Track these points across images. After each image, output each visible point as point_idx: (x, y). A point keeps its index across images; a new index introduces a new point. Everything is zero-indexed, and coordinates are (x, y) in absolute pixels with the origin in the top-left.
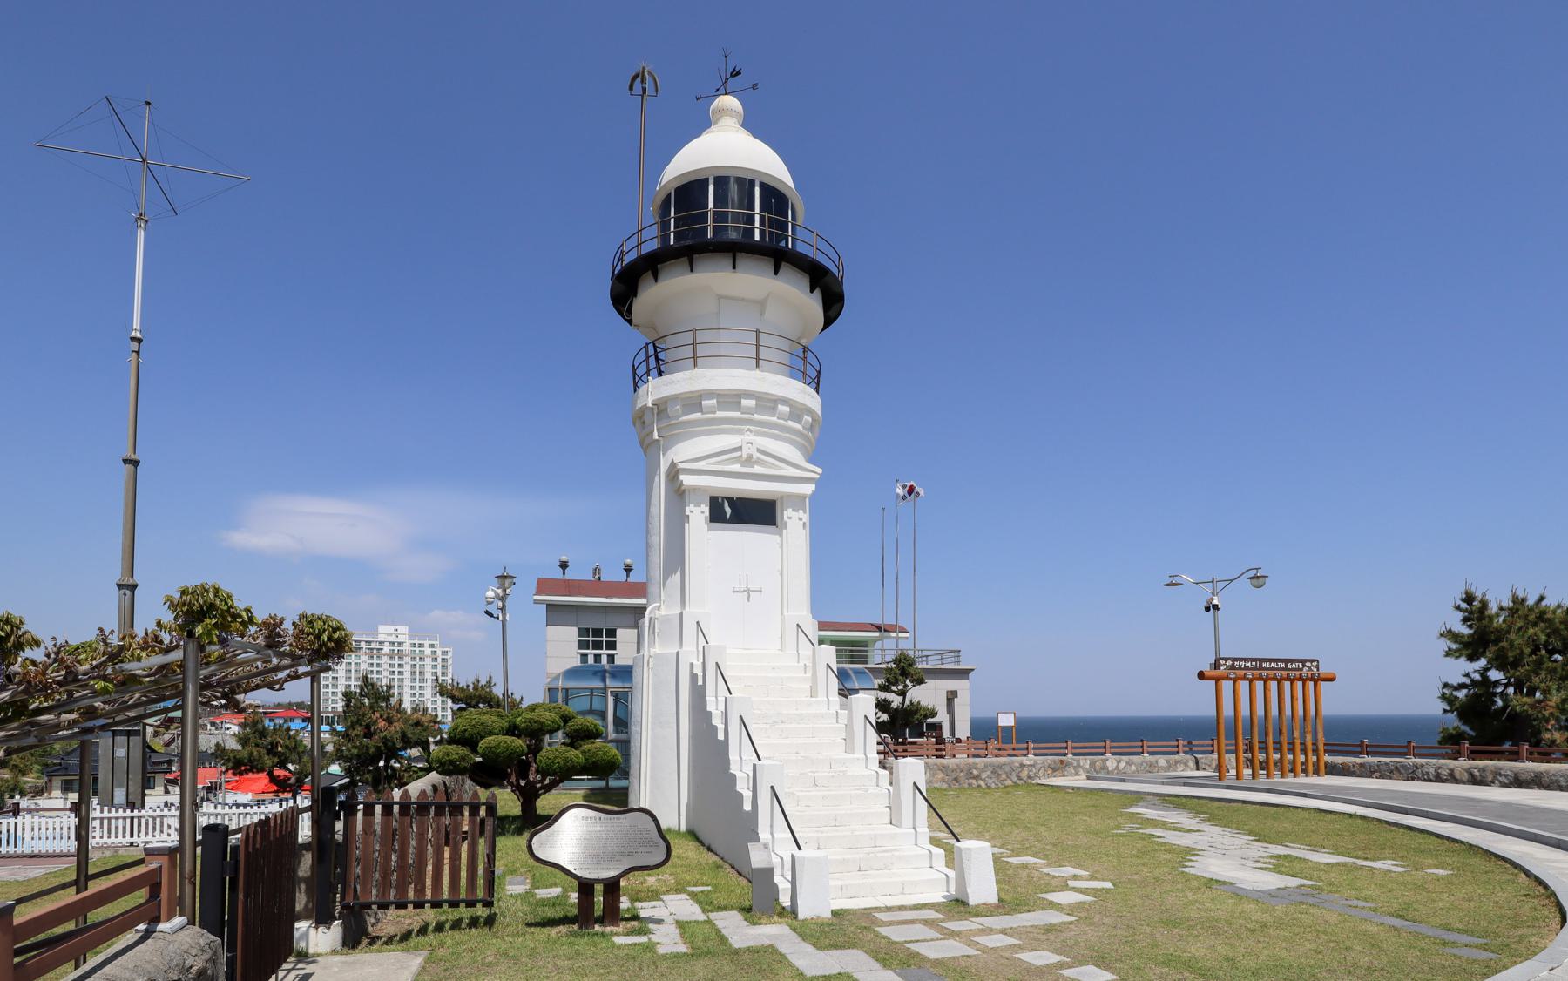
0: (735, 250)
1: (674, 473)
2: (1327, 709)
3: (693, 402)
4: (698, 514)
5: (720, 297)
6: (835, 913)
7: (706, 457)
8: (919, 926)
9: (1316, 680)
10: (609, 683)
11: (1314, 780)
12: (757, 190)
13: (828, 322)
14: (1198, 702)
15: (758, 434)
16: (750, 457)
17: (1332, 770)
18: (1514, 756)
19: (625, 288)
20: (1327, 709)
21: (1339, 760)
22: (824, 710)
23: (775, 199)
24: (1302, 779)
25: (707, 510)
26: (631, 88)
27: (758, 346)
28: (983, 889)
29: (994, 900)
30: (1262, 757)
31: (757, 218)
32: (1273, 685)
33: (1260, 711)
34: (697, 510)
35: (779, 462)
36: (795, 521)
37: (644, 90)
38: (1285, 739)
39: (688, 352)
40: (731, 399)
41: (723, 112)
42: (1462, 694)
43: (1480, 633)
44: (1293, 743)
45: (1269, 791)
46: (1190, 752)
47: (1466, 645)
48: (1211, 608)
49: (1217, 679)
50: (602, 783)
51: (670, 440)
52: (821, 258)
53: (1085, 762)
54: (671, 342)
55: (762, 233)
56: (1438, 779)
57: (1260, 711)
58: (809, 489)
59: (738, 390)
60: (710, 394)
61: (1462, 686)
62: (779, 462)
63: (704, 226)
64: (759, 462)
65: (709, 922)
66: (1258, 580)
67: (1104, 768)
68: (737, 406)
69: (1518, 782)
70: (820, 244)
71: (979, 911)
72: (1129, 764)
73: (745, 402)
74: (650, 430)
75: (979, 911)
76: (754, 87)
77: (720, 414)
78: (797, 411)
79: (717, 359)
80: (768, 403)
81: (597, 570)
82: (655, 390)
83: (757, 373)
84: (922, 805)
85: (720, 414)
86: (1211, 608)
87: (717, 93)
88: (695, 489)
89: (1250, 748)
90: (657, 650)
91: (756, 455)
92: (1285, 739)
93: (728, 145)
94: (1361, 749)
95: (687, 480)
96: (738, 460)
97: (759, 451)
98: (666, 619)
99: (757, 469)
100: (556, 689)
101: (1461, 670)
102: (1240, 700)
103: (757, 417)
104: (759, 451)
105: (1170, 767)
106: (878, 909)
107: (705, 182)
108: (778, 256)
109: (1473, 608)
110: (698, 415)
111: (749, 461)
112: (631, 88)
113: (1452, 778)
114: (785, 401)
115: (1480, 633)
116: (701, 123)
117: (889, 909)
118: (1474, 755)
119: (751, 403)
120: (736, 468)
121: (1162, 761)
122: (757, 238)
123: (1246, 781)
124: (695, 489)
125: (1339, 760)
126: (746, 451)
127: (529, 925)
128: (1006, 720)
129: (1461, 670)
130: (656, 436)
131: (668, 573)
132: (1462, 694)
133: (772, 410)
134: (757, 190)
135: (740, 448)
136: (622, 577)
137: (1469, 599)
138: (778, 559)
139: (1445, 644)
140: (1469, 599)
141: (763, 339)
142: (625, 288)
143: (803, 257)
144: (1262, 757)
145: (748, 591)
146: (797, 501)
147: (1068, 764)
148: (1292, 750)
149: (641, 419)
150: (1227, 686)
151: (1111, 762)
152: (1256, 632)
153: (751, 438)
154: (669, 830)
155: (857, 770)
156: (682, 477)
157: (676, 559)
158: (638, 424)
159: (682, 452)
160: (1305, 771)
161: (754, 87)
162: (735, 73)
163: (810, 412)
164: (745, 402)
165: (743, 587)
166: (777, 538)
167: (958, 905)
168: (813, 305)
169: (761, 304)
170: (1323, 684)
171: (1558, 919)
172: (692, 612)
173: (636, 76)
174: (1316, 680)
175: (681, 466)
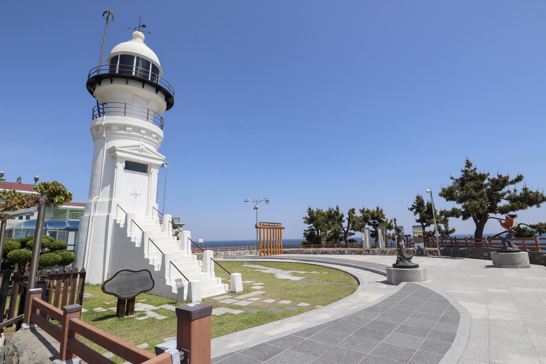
0: (143, 81)
1: (112, 152)
2: (284, 238)
3: (123, 127)
4: (121, 166)
5: (134, 95)
6: (203, 300)
7: (126, 146)
8: (229, 299)
9: (281, 229)
10: (48, 227)
11: (280, 255)
12: (135, 60)
13: (167, 110)
14: (252, 235)
15: (145, 142)
16: (142, 149)
17: (285, 253)
18: (310, 247)
19: (93, 83)
20: (284, 238)
21: (285, 250)
22: (167, 236)
23: (155, 68)
24: (278, 255)
25: (124, 165)
26: (103, 15)
27: (148, 114)
28: (239, 288)
29: (242, 290)
30: (266, 250)
31: (134, 69)
32: (272, 230)
33: (262, 239)
34: (121, 165)
35: (148, 150)
36: (154, 172)
37: (108, 18)
38: (274, 245)
39: (123, 110)
40: (138, 129)
41: (138, 36)
42: (308, 232)
43: (312, 218)
44: (264, 246)
45: (274, 258)
46: (249, 249)
47: (309, 220)
48: (256, 208)
49: (260, 228)
50: (79, 275)
51: (110, 139)
52: (170, 92)
53: (223, 253)
54: (109, 105)
55: (136, 73)
56: (307, 253)
57: (262, 239)
58: (160, 163)
59: (135, 126)
60: (130, 126)
61: (308, 231)
62: (148, 150)
63: (123, 69)
64: (145, 151)
65: (161, 309)
66: (267, 201)
67: (228, 255)
68: (139, 132)
69: (323, 253)
70: (171, 88)
71: (240, 294)
72: (234, 253)
73: (142, 131)
74: (98, 135)
75: (240, 294)
76: (149, 33)
77: (132, 133)
78: (158, 137)
79: (132, 115)
80: (150, 133)
81: (19, 179)
82: (106, 120)
83: (147, 122)
84: (213, 262)
85: (132, 133)
86: (256, 208)
87: (135, 29)
88: (121, 157)
89: (263, 248)
90: (97, 214)
91: (144, 149)
92: (274, 245)
93: (137, 46)
94: (290, 247)
95: (119, 154)
96: (138, 150)
97: (146, 148)
98: (102, 203)
99: (144, 154)
100: (20, 230)
101: (307, 227)
102: (265, 235)
103: (145, 136)
104: (146, 148)
105: (245, 254)
106: (214, 297)
107: (133, 57)
108: (158, 89)
109: (310, 212)
110: (124, 132)
111: (142, 150)
112: (103, 15)
113: (310, 253)
114: (155, 133)
115: (312, 218)
116: (130, 38)
117: (217, 296)
118: (314, 247)
119: (144, 132)
120: (137, 152)
121: (242, 252)
122: (150, 79)
123: (262, 257)
124: (121, 157)
125: (285, 250)
126: (141, 147)
127: (152, 310)
128: (201, 241)
129: (307, 227)
130: (104, 136)
131: (104, 185)
132: (308, 232)
133: (151, 135)
134: (135, 60)
135: (139, 146)
136: (33, 182)
137: (310, 209)
138: (145, 185)
139: (304, 220)
140: (310, 209)
141: (150, 112)
142: (93, 83)
143: (166, 90)
144: (266, 250)
145: (136, 194)
146: (155, 166)
147: (218, 254)
148: (276, 248)
149: (97, 128)
150: (262, 230)
151: (230, 253)
152: (267, 215)
153: (143, 143)
154: (88, 284)
155: (186, 255)
156: (117, 152)
157: (109, 180)
158: (94, 130)
159: (117, 143)
160: (276, 253)
161: (149, 33)
162: (144, 26)
163: (161, 138)
164: (142, 131)
165: (134, 193)
166: (148, 177)
167: (233, 293)
168: (164, 104)
169: (148, 101)
170: (282, 230)
171: (356, 282)
172: (115, 201)
173: (106, 12)
174: (281, 229)
175: (117, 148)
